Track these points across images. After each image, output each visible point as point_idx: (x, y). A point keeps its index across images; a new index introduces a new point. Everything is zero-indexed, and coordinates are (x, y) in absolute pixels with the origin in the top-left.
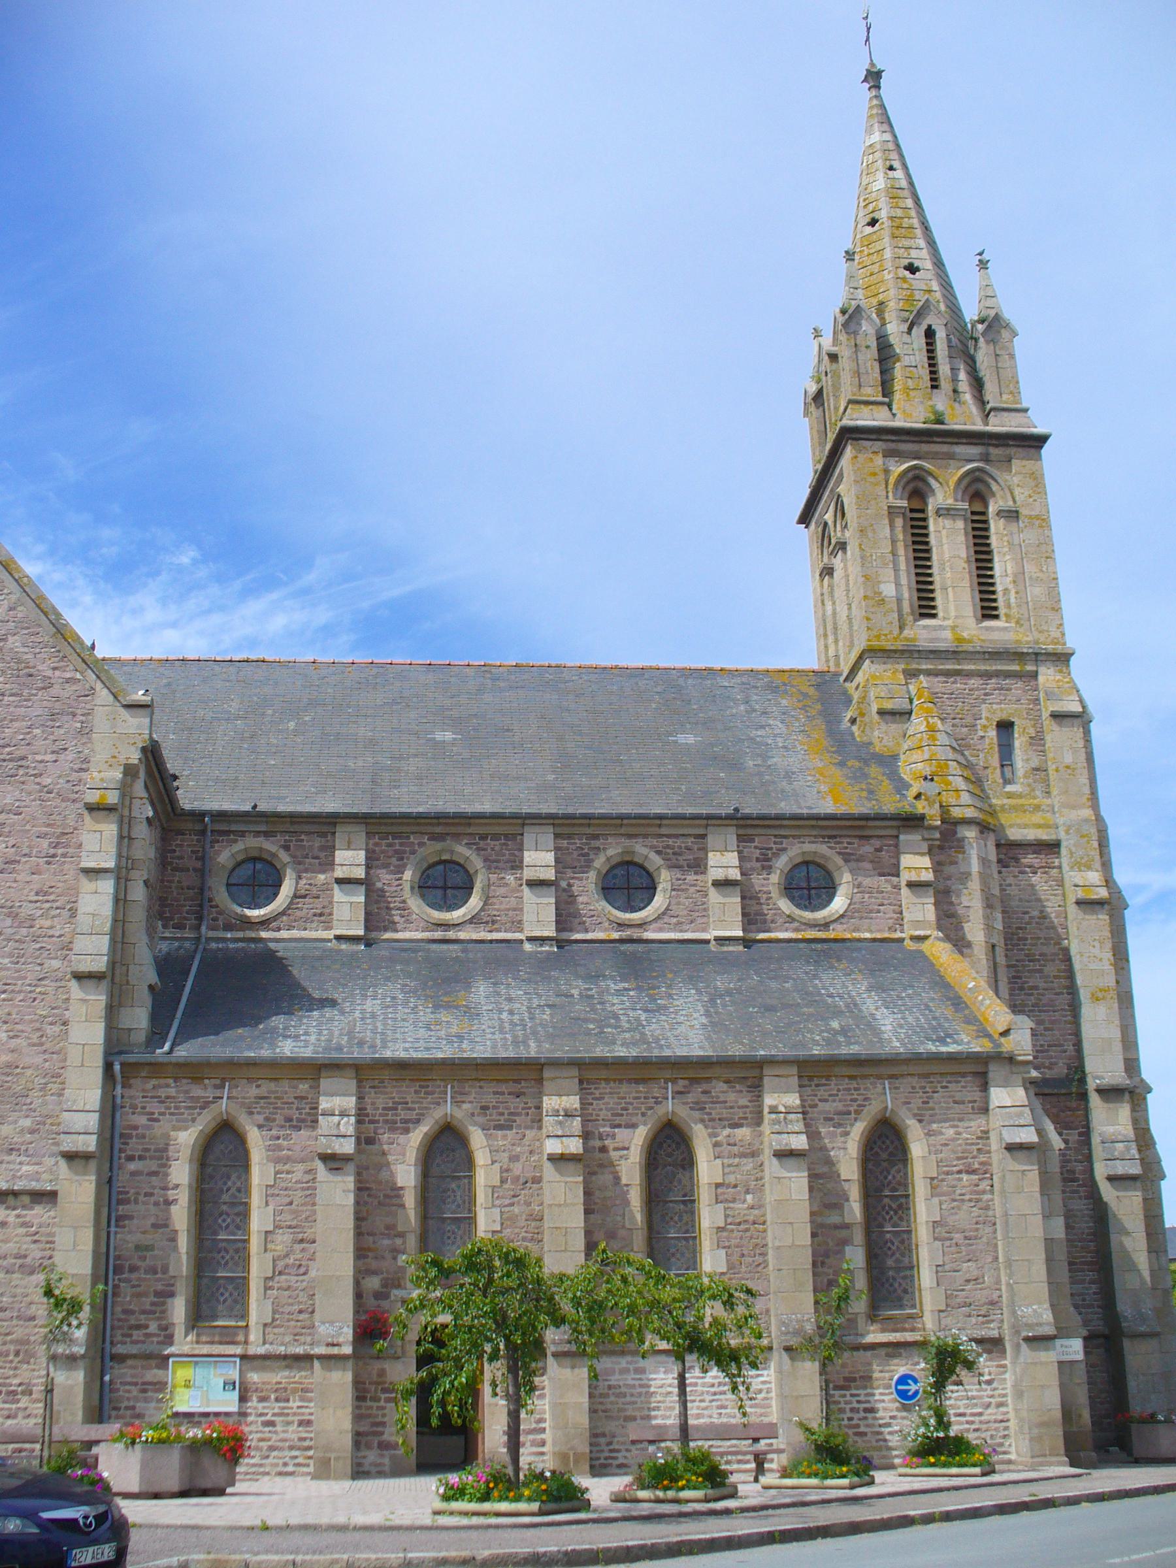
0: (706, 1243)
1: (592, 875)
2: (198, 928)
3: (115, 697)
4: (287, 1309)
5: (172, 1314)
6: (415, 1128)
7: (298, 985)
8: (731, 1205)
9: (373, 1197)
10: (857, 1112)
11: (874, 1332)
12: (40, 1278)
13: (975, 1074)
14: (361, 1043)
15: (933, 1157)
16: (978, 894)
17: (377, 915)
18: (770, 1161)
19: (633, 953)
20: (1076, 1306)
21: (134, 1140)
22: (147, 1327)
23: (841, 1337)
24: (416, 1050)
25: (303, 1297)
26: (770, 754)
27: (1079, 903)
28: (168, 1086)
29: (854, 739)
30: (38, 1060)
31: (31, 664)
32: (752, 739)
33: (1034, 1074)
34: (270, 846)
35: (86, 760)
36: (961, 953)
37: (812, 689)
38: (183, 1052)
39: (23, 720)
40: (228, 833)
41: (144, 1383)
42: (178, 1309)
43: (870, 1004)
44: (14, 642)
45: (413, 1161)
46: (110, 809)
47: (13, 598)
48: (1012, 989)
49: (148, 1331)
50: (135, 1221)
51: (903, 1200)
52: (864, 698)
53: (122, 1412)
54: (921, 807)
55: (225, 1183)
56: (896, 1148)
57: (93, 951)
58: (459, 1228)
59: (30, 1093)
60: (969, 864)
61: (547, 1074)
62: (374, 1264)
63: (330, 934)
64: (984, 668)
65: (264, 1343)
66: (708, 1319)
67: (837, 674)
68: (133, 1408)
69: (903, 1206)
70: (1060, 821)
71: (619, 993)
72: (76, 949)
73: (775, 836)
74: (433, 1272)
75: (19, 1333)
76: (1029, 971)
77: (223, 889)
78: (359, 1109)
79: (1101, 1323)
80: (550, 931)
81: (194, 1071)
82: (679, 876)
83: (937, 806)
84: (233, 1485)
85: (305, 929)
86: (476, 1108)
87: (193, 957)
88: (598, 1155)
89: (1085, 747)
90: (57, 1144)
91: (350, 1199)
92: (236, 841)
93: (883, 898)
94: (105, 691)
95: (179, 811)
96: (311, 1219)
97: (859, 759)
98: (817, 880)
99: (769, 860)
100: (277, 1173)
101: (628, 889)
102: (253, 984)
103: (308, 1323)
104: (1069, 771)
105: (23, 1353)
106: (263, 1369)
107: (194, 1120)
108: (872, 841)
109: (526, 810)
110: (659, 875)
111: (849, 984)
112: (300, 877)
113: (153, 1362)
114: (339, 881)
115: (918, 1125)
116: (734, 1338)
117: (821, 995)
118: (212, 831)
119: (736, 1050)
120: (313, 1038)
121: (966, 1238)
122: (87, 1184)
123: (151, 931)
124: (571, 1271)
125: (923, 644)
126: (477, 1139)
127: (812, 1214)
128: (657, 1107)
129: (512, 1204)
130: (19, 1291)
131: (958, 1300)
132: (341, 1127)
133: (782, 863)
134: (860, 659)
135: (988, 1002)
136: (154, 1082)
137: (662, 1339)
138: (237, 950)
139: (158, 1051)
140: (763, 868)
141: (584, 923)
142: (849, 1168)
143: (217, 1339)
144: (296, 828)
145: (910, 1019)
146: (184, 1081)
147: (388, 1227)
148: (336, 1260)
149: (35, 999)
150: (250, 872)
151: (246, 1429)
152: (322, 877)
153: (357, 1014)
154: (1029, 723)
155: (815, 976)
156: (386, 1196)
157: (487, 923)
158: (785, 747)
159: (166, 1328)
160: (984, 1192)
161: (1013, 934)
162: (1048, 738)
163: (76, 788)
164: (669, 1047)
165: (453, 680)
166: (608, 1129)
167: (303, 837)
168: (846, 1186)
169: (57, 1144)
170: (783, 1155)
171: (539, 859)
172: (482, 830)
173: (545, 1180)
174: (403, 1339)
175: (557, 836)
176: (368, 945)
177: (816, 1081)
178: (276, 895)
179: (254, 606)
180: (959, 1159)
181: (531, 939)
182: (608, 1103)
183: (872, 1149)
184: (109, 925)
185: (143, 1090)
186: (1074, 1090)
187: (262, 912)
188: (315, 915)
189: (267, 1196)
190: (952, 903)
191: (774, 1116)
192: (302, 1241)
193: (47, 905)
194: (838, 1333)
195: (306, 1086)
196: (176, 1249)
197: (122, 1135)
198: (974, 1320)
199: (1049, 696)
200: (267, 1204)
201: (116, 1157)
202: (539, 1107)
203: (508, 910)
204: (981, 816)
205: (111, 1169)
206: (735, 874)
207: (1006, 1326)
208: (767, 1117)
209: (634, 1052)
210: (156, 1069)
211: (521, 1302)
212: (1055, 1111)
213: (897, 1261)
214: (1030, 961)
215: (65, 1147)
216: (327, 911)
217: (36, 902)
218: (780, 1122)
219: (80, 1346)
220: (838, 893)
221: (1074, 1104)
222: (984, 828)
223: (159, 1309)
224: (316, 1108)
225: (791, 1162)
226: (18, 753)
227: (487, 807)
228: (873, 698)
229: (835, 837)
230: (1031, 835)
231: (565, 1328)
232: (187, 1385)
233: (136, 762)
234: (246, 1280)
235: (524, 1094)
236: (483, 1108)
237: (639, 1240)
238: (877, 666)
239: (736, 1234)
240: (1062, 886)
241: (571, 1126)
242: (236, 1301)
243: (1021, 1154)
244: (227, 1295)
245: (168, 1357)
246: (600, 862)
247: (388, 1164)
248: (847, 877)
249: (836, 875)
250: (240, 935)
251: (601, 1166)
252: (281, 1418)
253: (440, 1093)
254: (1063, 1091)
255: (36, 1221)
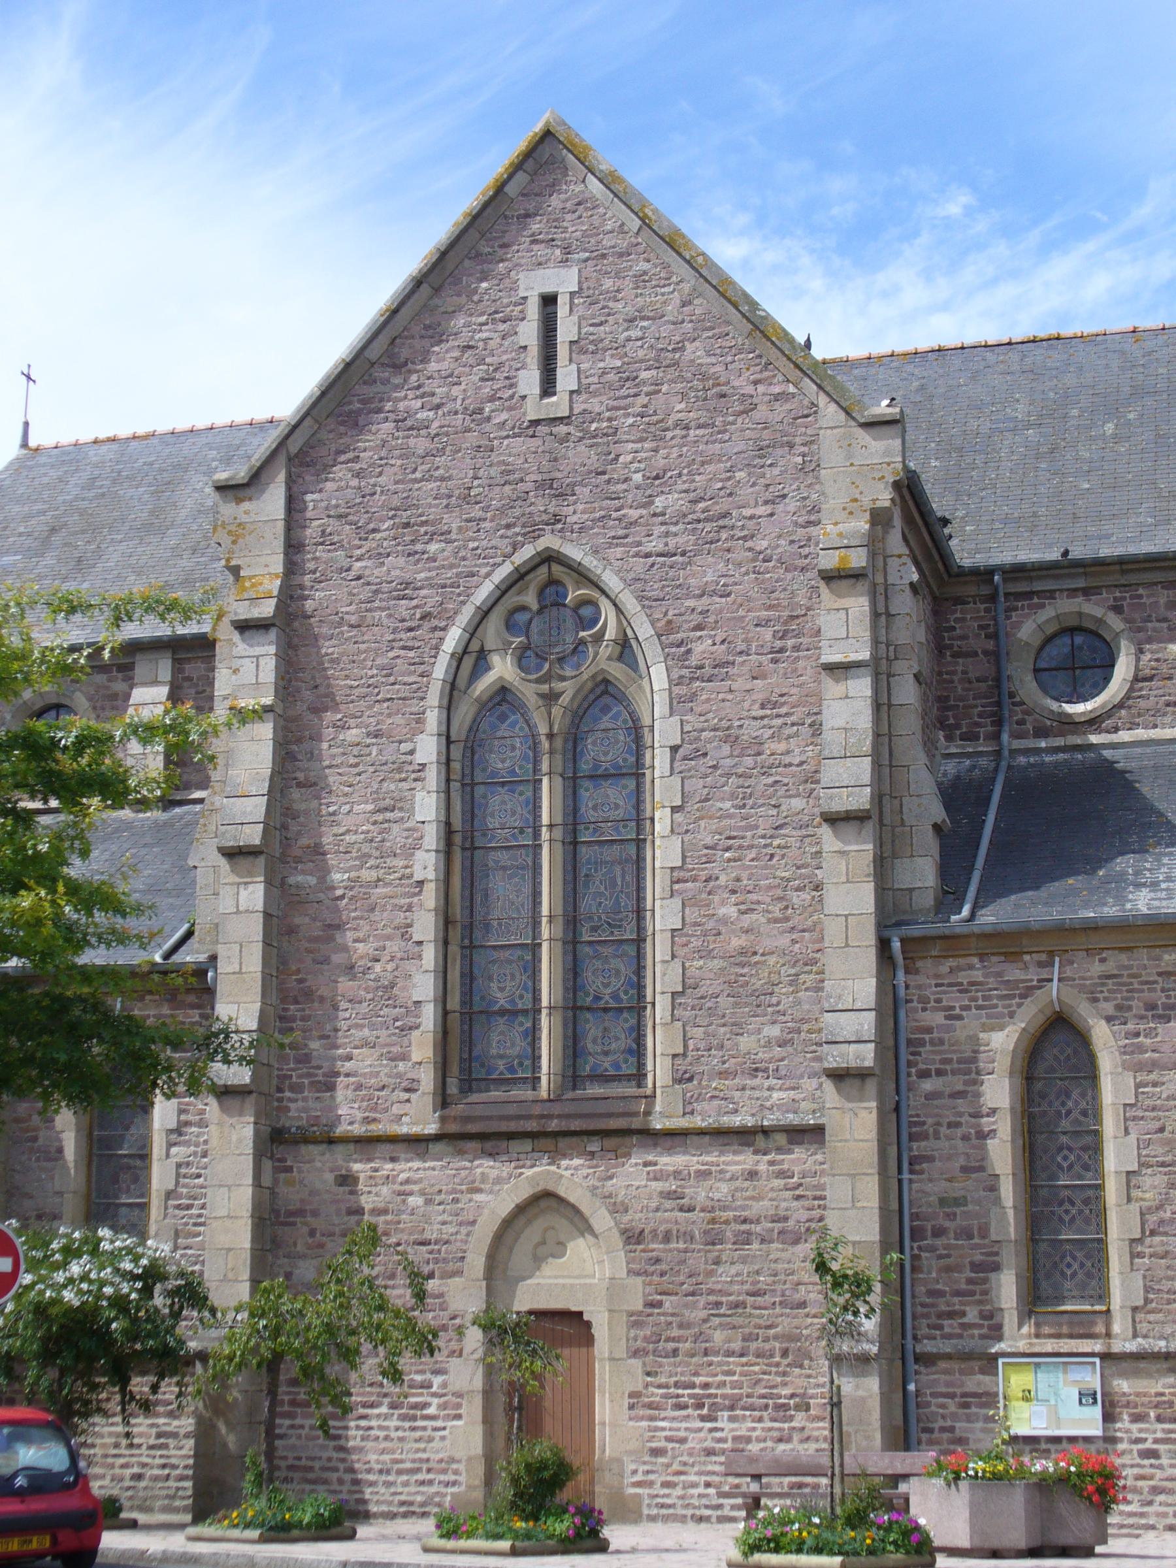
2: (997, 736)
3: (848, 413)
5: (998, 1297)
12: (806, 1249)
21: (928, 1048)
22: (964, 1314)
28: (971, 967)
30: (784, 941)
31: (722, 380)
34: (1093, 608)
35: (815, 509)
38: (989, 917)
39: (720, 461)
40: (1029, 595)
41: (964, 1395)
42: (1007, 1289)
44: (695, 351)
46: (856, 576)
47: (686, 287)
49: (965, 1320)
50: (938, 1164)
53: (936, 1435)
55: (1063, 1104)
57: (850, 780)
59: (776, 989)
65: (1135, 1336)
68: (951, 1429)
72: (826, 778)
75: (785, 1325)
77: (1029, 678)
81: (1007, 944)
84: (1105, 1542)
85: (1155, 726)
90: (819, 1059)
92: (1043, 606)
94: (833, 407)
105: (794, 1353)
106: (1136, 1374)
107: (1011, 1015)
112: (1141, 651)
113: (976, 1365)
118: (1006, 595)
122: (863, 1114)
123: (929, 745)
130: (780, 1266)
136: (952, 963)
138: (1056, 764)
139: (953, 918)
144: (1132, 578)
146: (994, 959)
149: (772, 856)
150: (1067, 650)
151: (1118, 1462)
159: (991, 1316)
163: (806, 551)
169: (819, 1059)
178: (1107, 680)
179: (1061, 267)
184: (868, 742)
185: (937, 976)
187: (1089, 706)
188: (1168, 705)
189: (1126, 1120)
193: (779, 721)
196: (998, 1201)
197: (910, 1042)
200: (1127, 1132)
201: (904, 1073)
205: (898, 1092)
210: (953, 944)
215: (830, 1063)
217: (762, 718)
219: (872, 1343)
223: (978, 1288)
226: (718, 509)
232: (1027, 1397)
233: (887, 504)
234: (1102, 1244)
242: (1089, 1275)
244: (1076, 1266)
245: (995, 1358)
250: (1059, 742)
252: (1167, 1447)
255: (796, 1169)
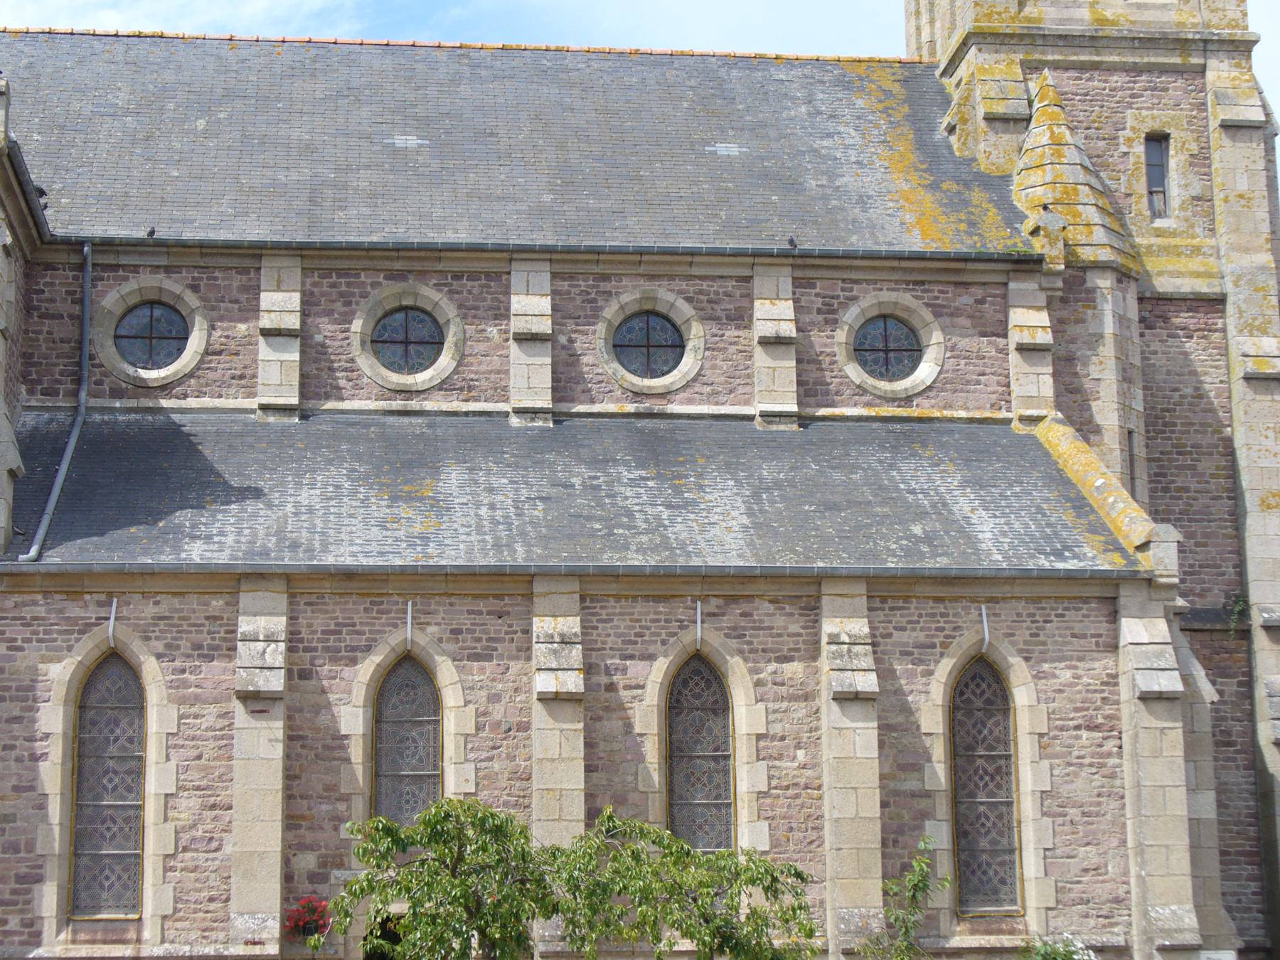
0: (744, 812)
1: (601, 328)
2: (75, 394)
4: (194, 896)
5: (40, 906)
6: (365, 658)
7: (212, 470)
8: (777, 763)
9: (308, 748)
10: (945, 645)
11: (960, 933)
13: (1102, 599)
14: (294, 546)
15: (1043, 707)
16: (1111, 364)
17: (317, 378)
18: (829, 709)
19: (653, 432)
20: (1229, 909)
23: (917, 938)
24: (367, 554)
25: (214, 880)
26: (838, 171)
27: (1248, 378)
28: (35, 603)
29: (952, 153)
32: (816, 151)
33: (1180, 602)
36: (1087, 440)
37: (897, 85)
38: (54, 558)
40: (116, 267)
42: (48, 898)
43: (963, 503)
45: (361, 702)
48: (1153, 491)
49: (7, 928)
51: (1002, 762)
52: (967, 98)
54: (1038, 246)
55: (112, 731)
56: (995, 694)
58: (421, 789)
60: (1101, 323)
61: (538, 587)
62: (309, 837)
63: (253, 403)
64: (1131, 59)
65: (163, 942)
66: (744, 911)
67: (932, 66)
69: (1001, 769)
70: (1227, 268)
71: (633, 483)
73: (844, 280)
74: (385, 843)
76: (1177, 467)
77: (110, 342)
78: (291, 633)
79: (1262, 932)
80: (545, 402)
81: (70, 584)
82: (715, 331)
83: (1060, 245)
85: (220, 396)
86: (444, 631)
87: (69, 433)
88: (604, 695)
89: (1267, 169)
91: (279, 751)
92: (126, 279)
93: (985, 365)
95: (48, 238)
96: (226, 778)
97: (957, 180)
98: (898, 339)
99: (833, 312)
100: (181, 717)
101: (648, 346)
102: (150, 467)
103: (221, 914)
104: (1243, 202)
107: (70, 649)
108: (973, 290)
109: (514, 240)
110: (689, 329)
111: (936, 477)
112: (213, 328)
114: (266, 333)
115: (1023, 663)
116: (778, 937)
117: (898, 489)
118: (94, 265)
119: (786, 561)
120: (230, 539)
121: (1084, 814)
124: (566, 845)
125: (1050, 26)
126: (446, 672)
127: (882, 777)
128: (681, 633)
129: (491, 759)
131: (1072, 895)
132: (267, 656)
133: (852, 315)
134: (964, 46)
135: (1121, 505)
136: (17, 598)
137: (684, 935)
138: (129, 424)
139: (21, 557)
140: (827, 322)
141: (589, 390)
142: (931, 717)
143: (99, 936)
144: (210, 262)
145: (1017, 525)
146: (58, 597)
147: (328, 788)
148: (258, 831)
152: (242, 327)
153: (289, 508)
154: (1190, 136)
155: (892, 466)
156: (326, 747)
157: (461, 389)
158: (858, 163)
160: (1109, 755)
161: (1157, 417)
162: (1216, 156)
164: (699, 554)
165: (419, 66)
166: (618, 661)
167: (217, 274)
168: (928, 741)
170: (847, 699)
171: (531, 306)
172: (457, 267)
173: (534, 727)
174: (345, 932)
175: (554, 276)
176: (304, 417)
177: (890, 603)
178: (180, 351)
180: (1076, 710)
181: (519, 412)
182: (618, 627)
183: (962, 693)
186: (1233, 625)
188: (233, 378)
189: (168, 747)
190: (1076, 374)
191: (834, 647)
192: (213, 807)
194: (913, 933)
195: (221, 602)
196: (45, 819)
198: (1092, 922)
199: (1220, 98)
200: (168, 758)
202: (527, 631)
203: (490, 372)
204: (1120, 259)
206: (789, 330)
207: (1134, 931)
208: (826, 649)
209: (653, 560)
211: (501, 883)
212: (1207, 652)
213: (994, 842)
214: (1178, 453)
216: (249, 372)
218: (842, 656)
220: (925, 358)
221: (1232, 644)
222: (1123, 275)
223: (21, 898)
224: (235, 632)
225: (856, 708)
227: (462, 236)
228: (979, 99)
229: (923, 283)
230: (1186, 286)
231: (557, 919)
235: (508, 613)
236: (453, 631)
237: (656, 807)
238: (986, 56)
239: (781, 801)
240: (1227, 355)
241: (568, 657)
242: (125, 887)
243: (1160, 707)
244: (113, 878)
246: (611, 311)
247: (328, 705)
248: (937, 336)
249: (922, 333)
250: (133, 403)
251: (608, 709)
253: (397, 611)
254: (1218, 627)
